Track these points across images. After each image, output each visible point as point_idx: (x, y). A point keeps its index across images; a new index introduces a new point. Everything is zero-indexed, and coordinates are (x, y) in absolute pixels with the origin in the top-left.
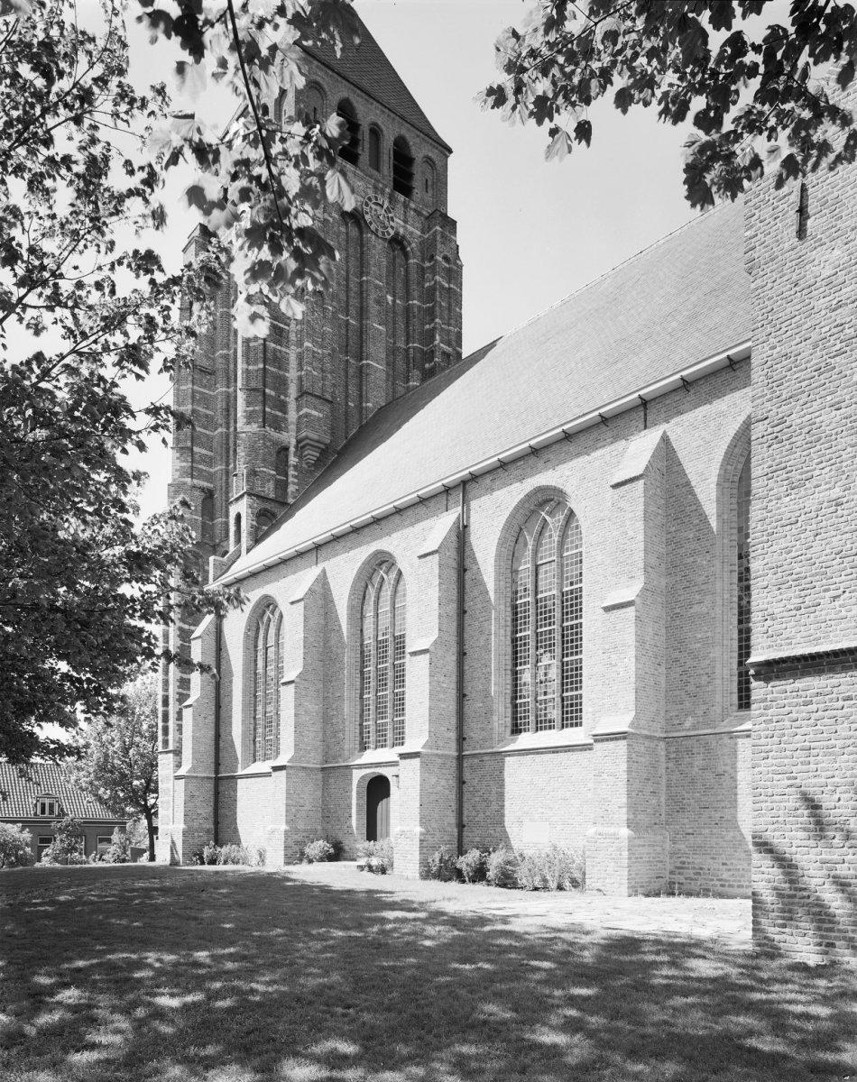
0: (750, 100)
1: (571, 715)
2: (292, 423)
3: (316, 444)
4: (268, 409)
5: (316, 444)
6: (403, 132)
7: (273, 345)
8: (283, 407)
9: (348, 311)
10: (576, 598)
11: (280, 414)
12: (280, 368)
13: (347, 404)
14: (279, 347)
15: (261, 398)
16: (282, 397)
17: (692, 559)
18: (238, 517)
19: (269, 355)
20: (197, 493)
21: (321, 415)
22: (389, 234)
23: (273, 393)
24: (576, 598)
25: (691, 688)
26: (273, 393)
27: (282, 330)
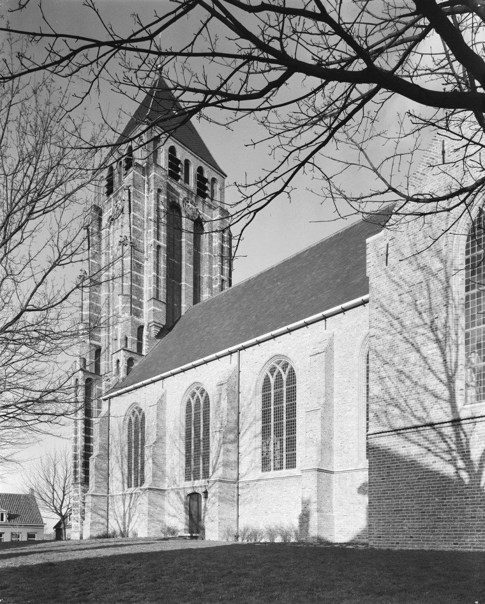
0: (272, 472)
1: (291, 463)
2: (451, 54)
3: (158, 325)
4: (133, 306)
5: (158, 325)
6: (202, 165)
7: (136, 273)
8: (141, 305)
9: (174, 256)
10: (293, 391)
11: (139, 309)
12: (139, 285)
13: (173, 305)
14: (139, 274)
15: (130, 300)
16: (140, 300)
17: (346, 391)
18: (118, 361)
19: (134, 278)
20: (93, 348)
21: (161, 310)
22: (195, 217)
23: (136, 298)
24: (293, 391)
25: (346, 449)
26: (136, 298)
27: (140, 266)
